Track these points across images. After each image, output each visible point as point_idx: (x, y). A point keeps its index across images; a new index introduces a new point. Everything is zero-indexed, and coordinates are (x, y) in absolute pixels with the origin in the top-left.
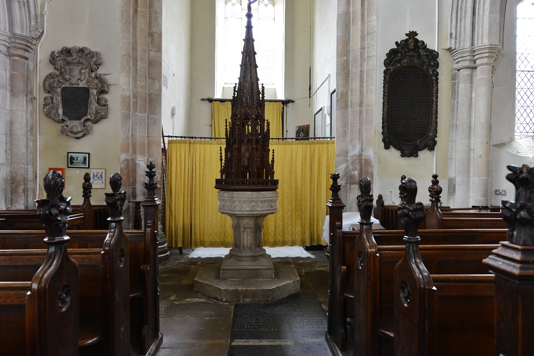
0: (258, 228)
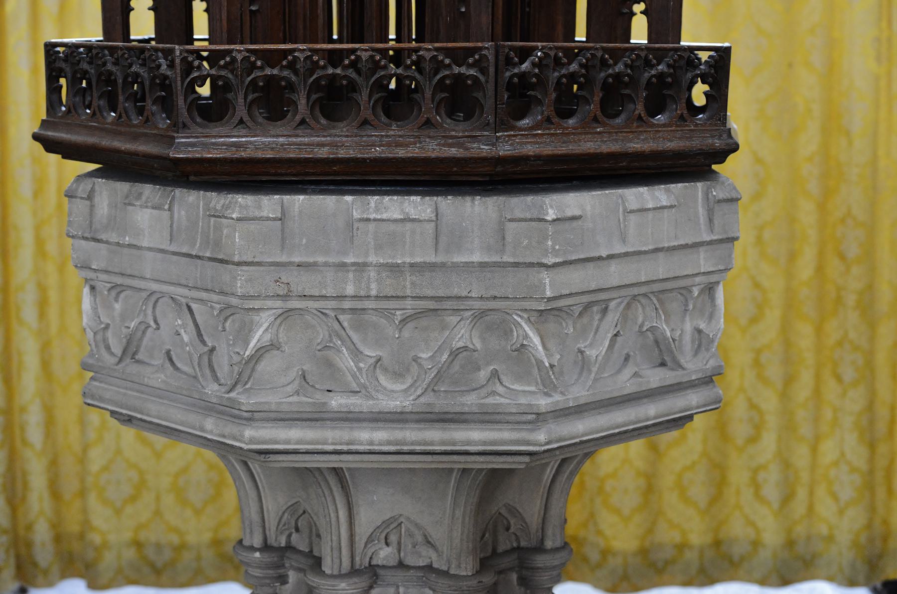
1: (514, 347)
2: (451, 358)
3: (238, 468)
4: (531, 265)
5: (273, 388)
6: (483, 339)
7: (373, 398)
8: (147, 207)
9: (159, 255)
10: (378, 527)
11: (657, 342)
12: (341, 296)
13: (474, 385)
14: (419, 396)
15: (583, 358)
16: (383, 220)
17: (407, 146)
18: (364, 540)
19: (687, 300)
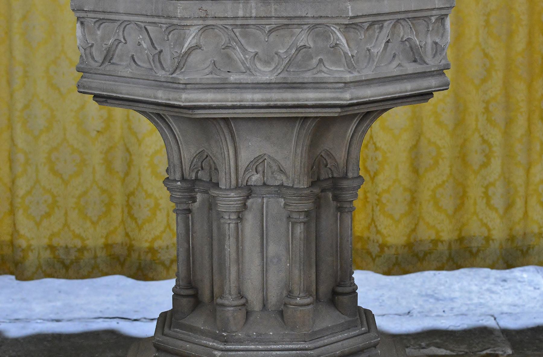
0: (330, 188)
6: (314, 42)
10: (252, 162)
11: (411, 47)
12: (236, 17)
13: (309, 68)
14: (280, 74)
19: (428, 25)
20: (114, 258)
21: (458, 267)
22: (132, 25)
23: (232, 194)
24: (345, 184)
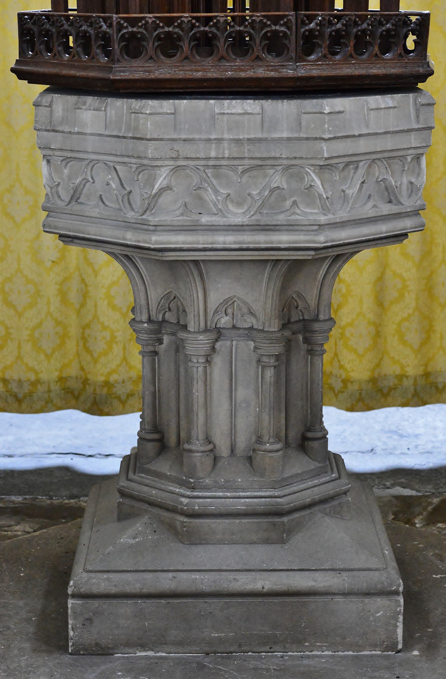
0: (301, 330)
1: (306, 187)
2: (270, 194)
3: (133, 272)
4: (316, 139)
5: (167, 212)
7: (225, 217)
8: (90, 110)
9: (97, 138)
10: (221, 304)
11: (387, 189)
14: (252, 215)
15: (345, 195)
16: (232, 114)
17: (246, 71)
18: (212, 313)
20: (68, 392)
21: (424, 403)
22: (100, 164)
23: (201, 337)
24: (317, 326)
